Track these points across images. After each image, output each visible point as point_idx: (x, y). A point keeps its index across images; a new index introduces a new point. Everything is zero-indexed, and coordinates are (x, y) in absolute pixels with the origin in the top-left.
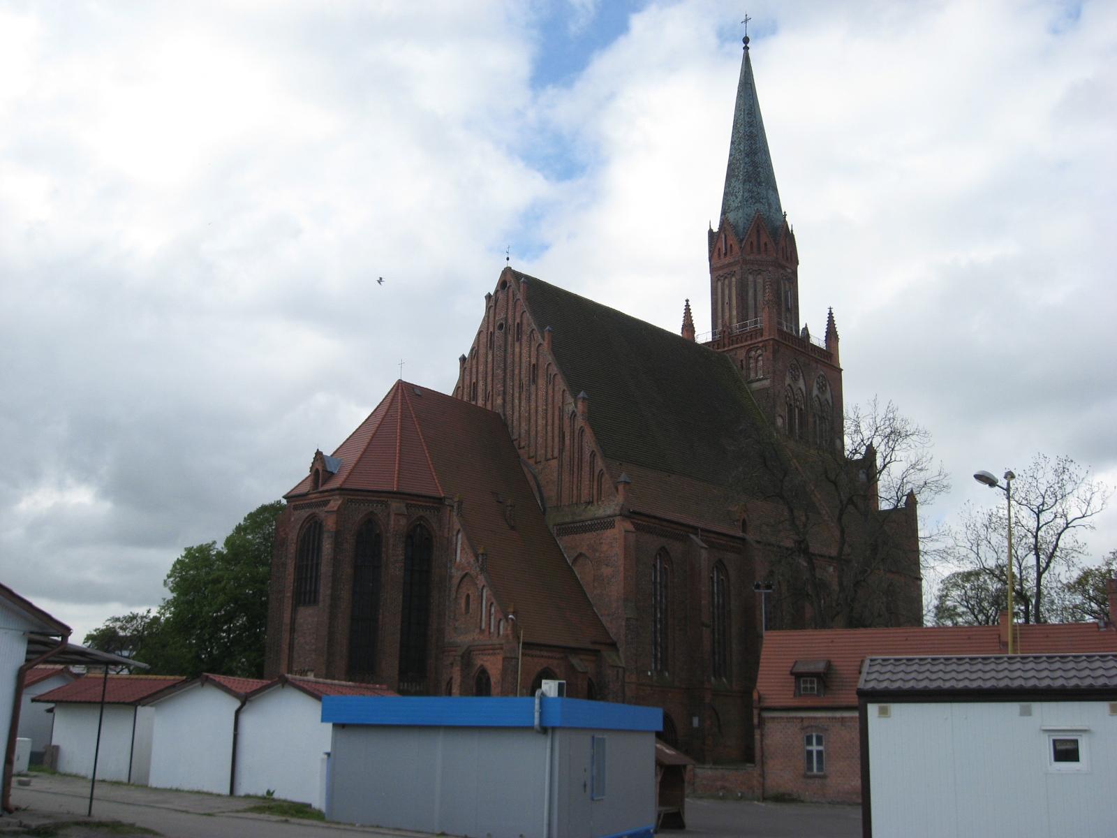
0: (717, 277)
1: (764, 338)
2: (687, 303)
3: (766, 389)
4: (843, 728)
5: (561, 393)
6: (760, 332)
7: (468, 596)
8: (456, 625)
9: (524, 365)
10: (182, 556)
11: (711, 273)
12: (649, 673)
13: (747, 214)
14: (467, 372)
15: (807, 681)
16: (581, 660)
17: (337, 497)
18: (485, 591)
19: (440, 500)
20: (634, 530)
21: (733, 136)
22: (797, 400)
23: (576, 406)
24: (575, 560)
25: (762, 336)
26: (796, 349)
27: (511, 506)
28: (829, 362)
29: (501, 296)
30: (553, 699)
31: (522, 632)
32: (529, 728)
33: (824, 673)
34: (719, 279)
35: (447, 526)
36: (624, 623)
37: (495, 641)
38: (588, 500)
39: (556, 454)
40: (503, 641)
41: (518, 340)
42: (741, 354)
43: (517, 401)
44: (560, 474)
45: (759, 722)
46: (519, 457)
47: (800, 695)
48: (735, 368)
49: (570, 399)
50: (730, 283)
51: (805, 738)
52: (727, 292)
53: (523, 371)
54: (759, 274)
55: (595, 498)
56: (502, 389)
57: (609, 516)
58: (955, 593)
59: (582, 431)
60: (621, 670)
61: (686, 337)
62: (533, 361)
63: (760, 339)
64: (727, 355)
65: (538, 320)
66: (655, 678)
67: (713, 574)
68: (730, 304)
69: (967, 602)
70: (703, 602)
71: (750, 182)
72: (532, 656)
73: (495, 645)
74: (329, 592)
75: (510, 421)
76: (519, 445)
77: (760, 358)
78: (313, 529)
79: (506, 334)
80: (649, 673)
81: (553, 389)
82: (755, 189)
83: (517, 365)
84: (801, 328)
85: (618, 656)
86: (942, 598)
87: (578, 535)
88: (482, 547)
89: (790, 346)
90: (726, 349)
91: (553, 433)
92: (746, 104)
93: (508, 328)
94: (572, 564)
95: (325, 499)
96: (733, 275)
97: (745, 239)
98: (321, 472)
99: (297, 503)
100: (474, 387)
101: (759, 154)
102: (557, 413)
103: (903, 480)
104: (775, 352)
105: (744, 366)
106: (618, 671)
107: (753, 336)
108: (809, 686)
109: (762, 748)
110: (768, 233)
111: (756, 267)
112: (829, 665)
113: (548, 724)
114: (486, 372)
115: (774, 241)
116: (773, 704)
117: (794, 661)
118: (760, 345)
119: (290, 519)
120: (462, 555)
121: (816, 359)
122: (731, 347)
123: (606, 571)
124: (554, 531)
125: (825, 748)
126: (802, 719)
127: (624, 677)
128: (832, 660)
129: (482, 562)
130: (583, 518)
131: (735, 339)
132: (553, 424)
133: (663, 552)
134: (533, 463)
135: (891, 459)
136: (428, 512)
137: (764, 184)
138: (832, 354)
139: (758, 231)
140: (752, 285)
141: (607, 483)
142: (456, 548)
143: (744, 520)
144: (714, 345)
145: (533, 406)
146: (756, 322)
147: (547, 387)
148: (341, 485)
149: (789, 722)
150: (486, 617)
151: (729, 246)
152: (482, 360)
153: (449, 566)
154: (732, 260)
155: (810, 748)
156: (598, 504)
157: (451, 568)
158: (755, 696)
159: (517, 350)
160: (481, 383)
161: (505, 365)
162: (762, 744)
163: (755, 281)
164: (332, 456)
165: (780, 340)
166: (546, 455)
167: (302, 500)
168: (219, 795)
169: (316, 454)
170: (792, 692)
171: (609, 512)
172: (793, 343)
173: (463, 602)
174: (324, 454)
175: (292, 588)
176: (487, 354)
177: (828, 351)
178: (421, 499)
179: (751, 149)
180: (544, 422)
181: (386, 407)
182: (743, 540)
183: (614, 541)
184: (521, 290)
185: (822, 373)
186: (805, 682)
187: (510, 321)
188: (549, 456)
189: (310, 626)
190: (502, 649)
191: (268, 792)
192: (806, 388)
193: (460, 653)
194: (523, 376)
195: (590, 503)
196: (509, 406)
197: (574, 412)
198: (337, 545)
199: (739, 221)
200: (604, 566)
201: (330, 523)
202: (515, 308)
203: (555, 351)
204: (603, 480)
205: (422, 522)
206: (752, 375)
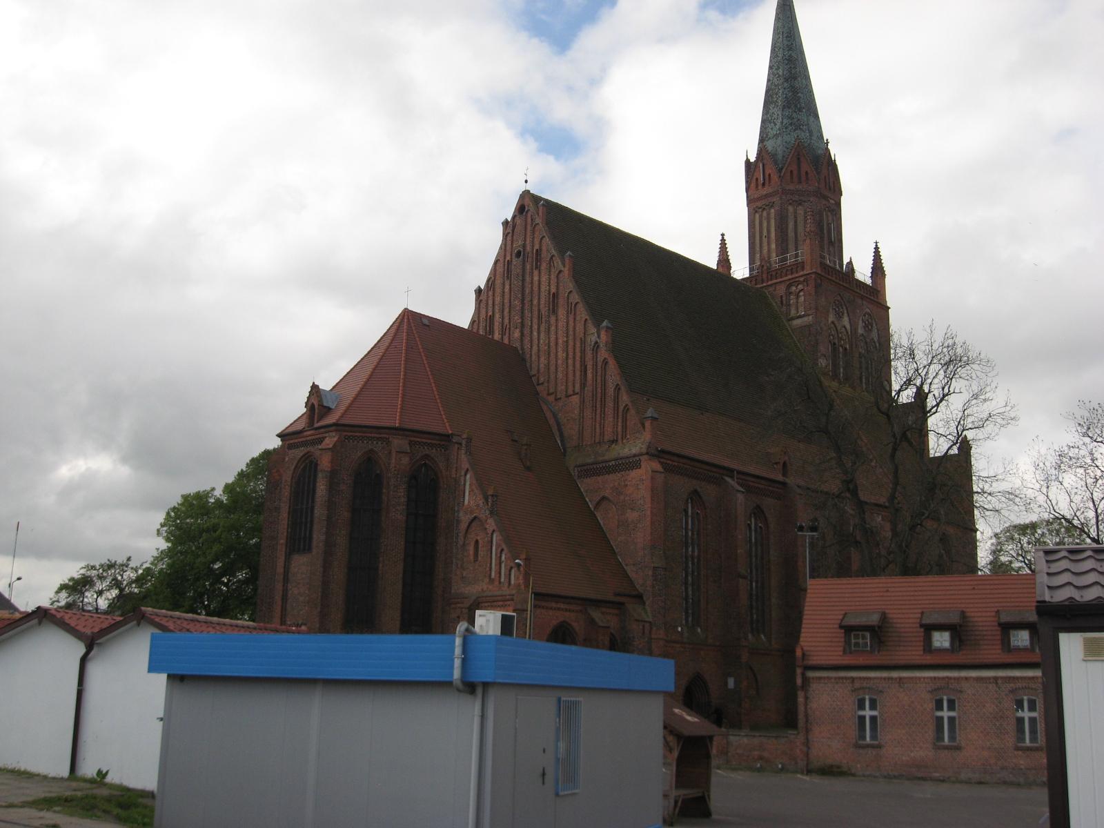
0: (754, 209)
1: (805, 272)
2: (723, 238)
3: (809, 326)
4: (902, 690)
5: (583, 323)
6: (802, 265)
7: (477, 542)
8: (464, 575)
9: (543, 295)
10: (178, 504)
11: (748, 205)
12: (680, 629)
13: (786, 142)
14: (483, 305)
15: (858, 635)
16: (603, 613)
17: (334, 434)
18: (495, 535)
19: (447, 437)
20: (662, 470)
21: (771, 61)
22: (841, 339)
23: (599, 337)
24: (598, 504)
25: (803, 270)
26: (839, 284)
27: (527, 445)
28: (875, 300)
29: (518, 221)
30: (488, 638)
31: (531, 578)
32: (446, 685)
33: (879, 627)
34: (756, 212)
35: (455, 466)
36: (650, 573)
37: (506, 591)
38: (612, 439)
39: (577, 389)
40: (514, 592)
41: (536, 268)
42: (781, 290)
43: (535, 334)
44: (582, 410)
45: (803, 682)
46: (538, 394)
47: (851, 653)
48: (774, 304)
49: (592, 329)
50: (769, 214)
51: (856, 701)
52: (765, 225)
53: (543, 302)
54: (800, 204)
55: (620, 437)
56: (520, 321)
57: (635, 456)
58: (1010, 547)
59: (605, 362)
60: (647, 625)
61: (721, 270)
62: (553, 290)
63: (801, 273)
64: (766, 291)
65: (554, 245)
66: (686, 635)
67: (751, 521)
68: (768, 237)
69: (1023, 557)
70: (739, 551)
71: (789, 108)
73: (505, 596)
74: (323, 538)
75: (528, 356)
76: (538, 381)
77: (802, 294)
78: (308, 467)
80: (680, 629)
81: (575, 319)
84: (845, 263)
86: (996, 552)
87: (601, 476)
88: (492, 487)
89: (834, 281)
90: (765, 284)
91: (574, 366)
92: (784, 27)
93: (526, 255)
94: (595, 508)
95: (321, 436)
96: (772, 206)
97: (785, 167)
98: (316, 406)
99: (292, 442)
100: (490, 321)
102: (578, 344)
103: (964, 412)
104: (817, 287)
105: (784, 302)
106: (644, 626)
107: (794, 270)
108: (861, 641)
110: (809, 161)
111: (796, 198)
112: (884, 617)
113: (480, 676)
114: (503, 302)
115: (816, 169)
116: (819, 662)
117: (843, 612)
118: (802, 279)
119: (284, 459)
120: (470, 498)
121: (862, 295)
122: (770, 283)
123: (632, 516)
124: (575, 473)
125: (880, 713)
126: (853, 679)
127: (650, 632)
128: (887, 611)
129: (492, 505)
130: (606, 458)
131: (774, 273)
132: (574, 358)
133: (695, 496)
134: (553, 400)
135: (949, 391)
136: (434, 450)
137: (804, 110)
138: (879, 291)
139: (799, 159)
140: (793, 217)
142: (464, 490)
143: (785, 464)
144: (751, 281)
145: (553, 337)
146: (797, 255)
147: (568, 317)
148: (338, 420)
149: (837, 683)
150: (496, 565)
151: (767, 176)
152: (498, 291)
153: (456, 509)
154: (770, 190)
155: (861, 713)
156: (623, 443)
157: (458, 511)
158: (799, 653)
159: (536, 278)
160: (497, 316)
161: (523, 295)
162: (806, 708)
163: (795, 212)
164: (331, 390)
165: (823, 274)
166: (566, 392)
167: (296, 438)
168: (62, 779)
169: (312, 387)
170: (841, 649)
171: (634, 451)
172: (836, 278)
173: (471, 549)
174: (320, 387)
175: (285, 534)
176: (504, 284)
177: (875, 287)
179: (791, 73)
180: (564, 355)
181: (391, 338)
182: (784, 484)
183: (640, 483)
184: (541, 214)
185: (868, 310)
186: (857, 637)
187: (528, 248)
188: (570, 392)
189: (304, 576)
190: (512, 600)
191: (99, 772)
192: (851, 326)
193: (468, 605)
194: (542, 306)
195: (614, 441)
196: (527, 341)
197: (596, 343)
198: (332, 487)
199: (779, 150)
201: (325, 462)
202: (533, 231)
203: (576, 276)
204: (628, 415)
205: (427, 462)
206: (793, 312)
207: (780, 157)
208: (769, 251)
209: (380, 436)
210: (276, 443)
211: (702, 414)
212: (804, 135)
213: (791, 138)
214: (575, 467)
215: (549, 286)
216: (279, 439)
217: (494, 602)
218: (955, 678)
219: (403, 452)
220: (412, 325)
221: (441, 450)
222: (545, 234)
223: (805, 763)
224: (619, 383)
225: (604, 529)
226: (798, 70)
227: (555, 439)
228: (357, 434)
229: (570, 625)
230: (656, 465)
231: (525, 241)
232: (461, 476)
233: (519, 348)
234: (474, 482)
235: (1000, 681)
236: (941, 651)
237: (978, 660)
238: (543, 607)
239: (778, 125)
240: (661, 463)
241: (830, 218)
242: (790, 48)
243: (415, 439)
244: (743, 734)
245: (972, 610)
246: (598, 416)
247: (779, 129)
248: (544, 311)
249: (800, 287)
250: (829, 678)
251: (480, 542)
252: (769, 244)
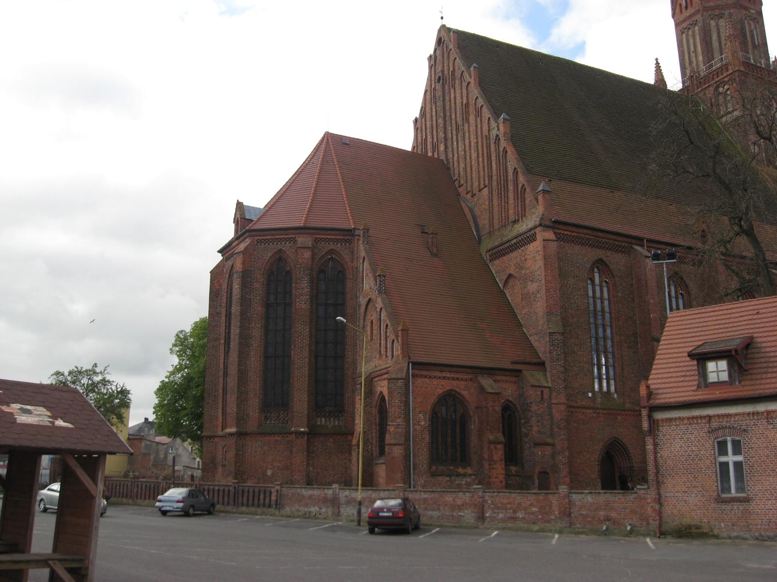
2: (657, 62)
3: (737, 119)
7: (372, 321)
14: (419, 132)
19: (350, 232)
23: (498, 130)
24: (506, 282)
34: (683, 33)
43: (455, 143)
44: (491, 200)
45: (650, 426)
49: (493, 124)
50: (693, 32)
51: (716, 444)
52: (691, 41)
56: (443, 136)
57: (531, 230)
68: (695, 51)
72: (430, 377)
74: (238, 331)
75: (451, 164)
77: (729, 92)
79: (443, 85)
83: (453, 111)
94: (503, 287)
96: (695, 24)
106: (542, 392)
109: (656, 461)
111: (717, 12)
118: (726, 79)
120: (368, 284)
123: (532, 287)
124: (486, 257)
126: (710, 418)
128: (755, 335)
129: (380, 285)
130: (509, 237)
141: (529, 196)
146: (722, 60)
147: (476, 120)
149: (690, 424)
154: (693, 11)
171: (531, 224)
183: (534, 257)
187: (446, 72)
197: (497, 136)
203: (482, 83)
209: (288, 236)
210: (219, 257)
211: (613, 192)
216: (220, 254)
217: (382, 375)
219: (304, 248)
221: (345, 244)
222: (456, 56)
223: (658, 522)
224: (516, 166)
228: (267, 237)
229: (459, 393)
230: (550, 235)
231: (443, 67)
233: (444, 160)
238: (426, 377)
241: (753, 26)
244: (587, 491)
249: (726, 87)
250: (681, 419)
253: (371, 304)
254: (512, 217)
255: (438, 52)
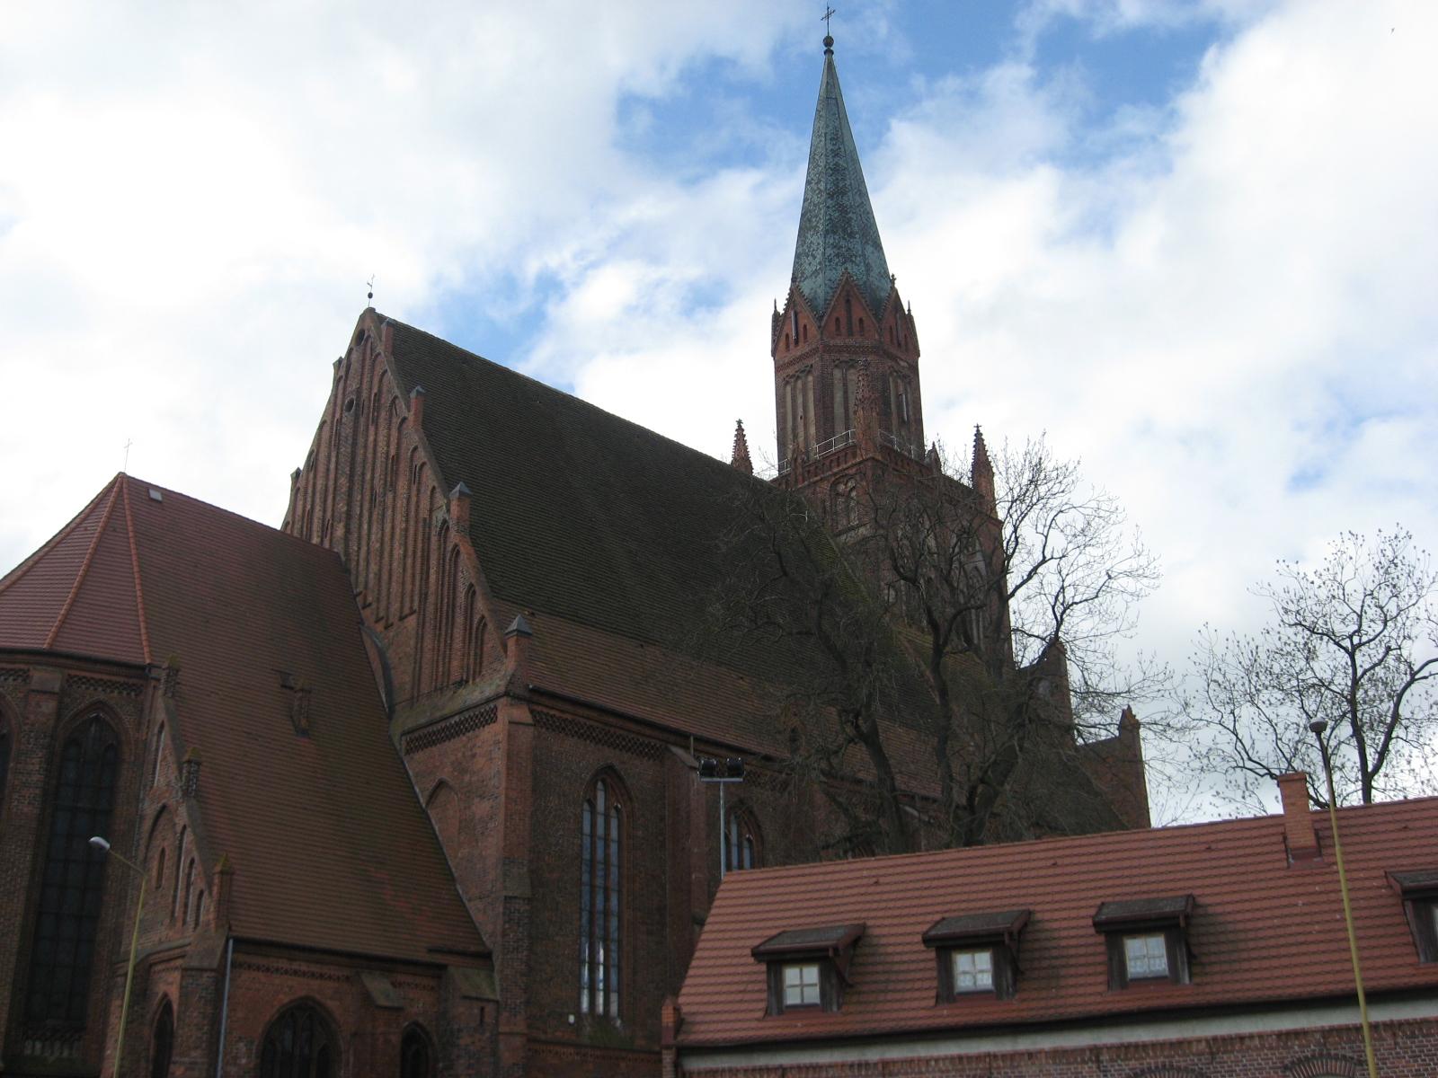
7: (163, 851)
12: (572, 1019)
14: (300, 496)
19: (141, 671)
21: (808, 173)
24: (432, 797)
34: (787, 383)
44: (420, 638)
49: (440, 500)
50: (804, 385)
52: (800, 400)
56: (345, 508)
57: (488, 701)
65: (430, 406)
68: (805, 417)
71: (835, 233)
77: (854, 494)
80: (572, 1019)
82: (843, 243)
83: (369, 466)
85: (491, 977)
92: (827, 126)
94: (427, 804)
96: (809, 372)
101: (850, 194)
106: (482, 1009)
107: (842, 459)
111: (845, 356)
115: (876, 315)
116: (709, 1036)
118: (852, 471)
120: (165, 777)
124: (401, 745)
129: (188, 780)
130: (446, 711)
131: (812, 468)
135: (1044, 557)
137: (857, 236)
139: (848, 301)
147: (409, 489)
151: (801, 330)
154: (807, 349)
171: (489, 691)
178: (98, 667)
184: (383, 339)
187: (365, 395)
194: (376, 481)
197: (445, 521)
199: (819, 291)
200: (477, 800)
203: (429, 424)
207: (821, 302)
208: (806, 438)
212: (856, 270)
213: (836, 274)
214: (402, 735)
215: (388, 446)
218: (1004, 1056)
219: (45, 692)
220: (125, 491)
222: (387, 367)
224: (473, 582)
225: (440, 838)
226: (848, 182)
227: (379, 692)
230: (522, 714)
232: (153, 735)
234: (169, 742)
235: (1105, 1057)
236: (976, 995)
237: (1052, 1011)
238: (258, 969)
239: (819, 257)
240: (532, 711)
241: (901, 389)
242: (836, 154)
243: (78, 673)
245: (1047, 907)
246: (442, 645)
247: (820, 263)
248: (378, 483)
251: (167, 852)
252: (806, 426)
253: (165, 815)
254: (456, 676)
255: (354, 356)
